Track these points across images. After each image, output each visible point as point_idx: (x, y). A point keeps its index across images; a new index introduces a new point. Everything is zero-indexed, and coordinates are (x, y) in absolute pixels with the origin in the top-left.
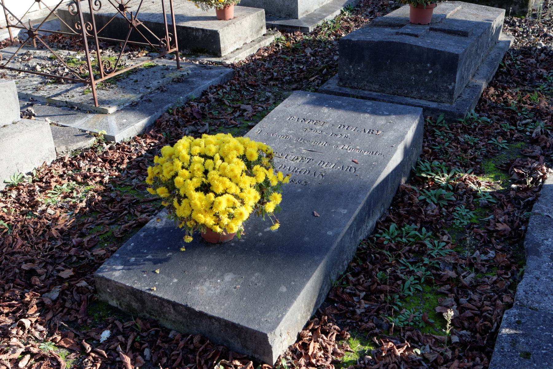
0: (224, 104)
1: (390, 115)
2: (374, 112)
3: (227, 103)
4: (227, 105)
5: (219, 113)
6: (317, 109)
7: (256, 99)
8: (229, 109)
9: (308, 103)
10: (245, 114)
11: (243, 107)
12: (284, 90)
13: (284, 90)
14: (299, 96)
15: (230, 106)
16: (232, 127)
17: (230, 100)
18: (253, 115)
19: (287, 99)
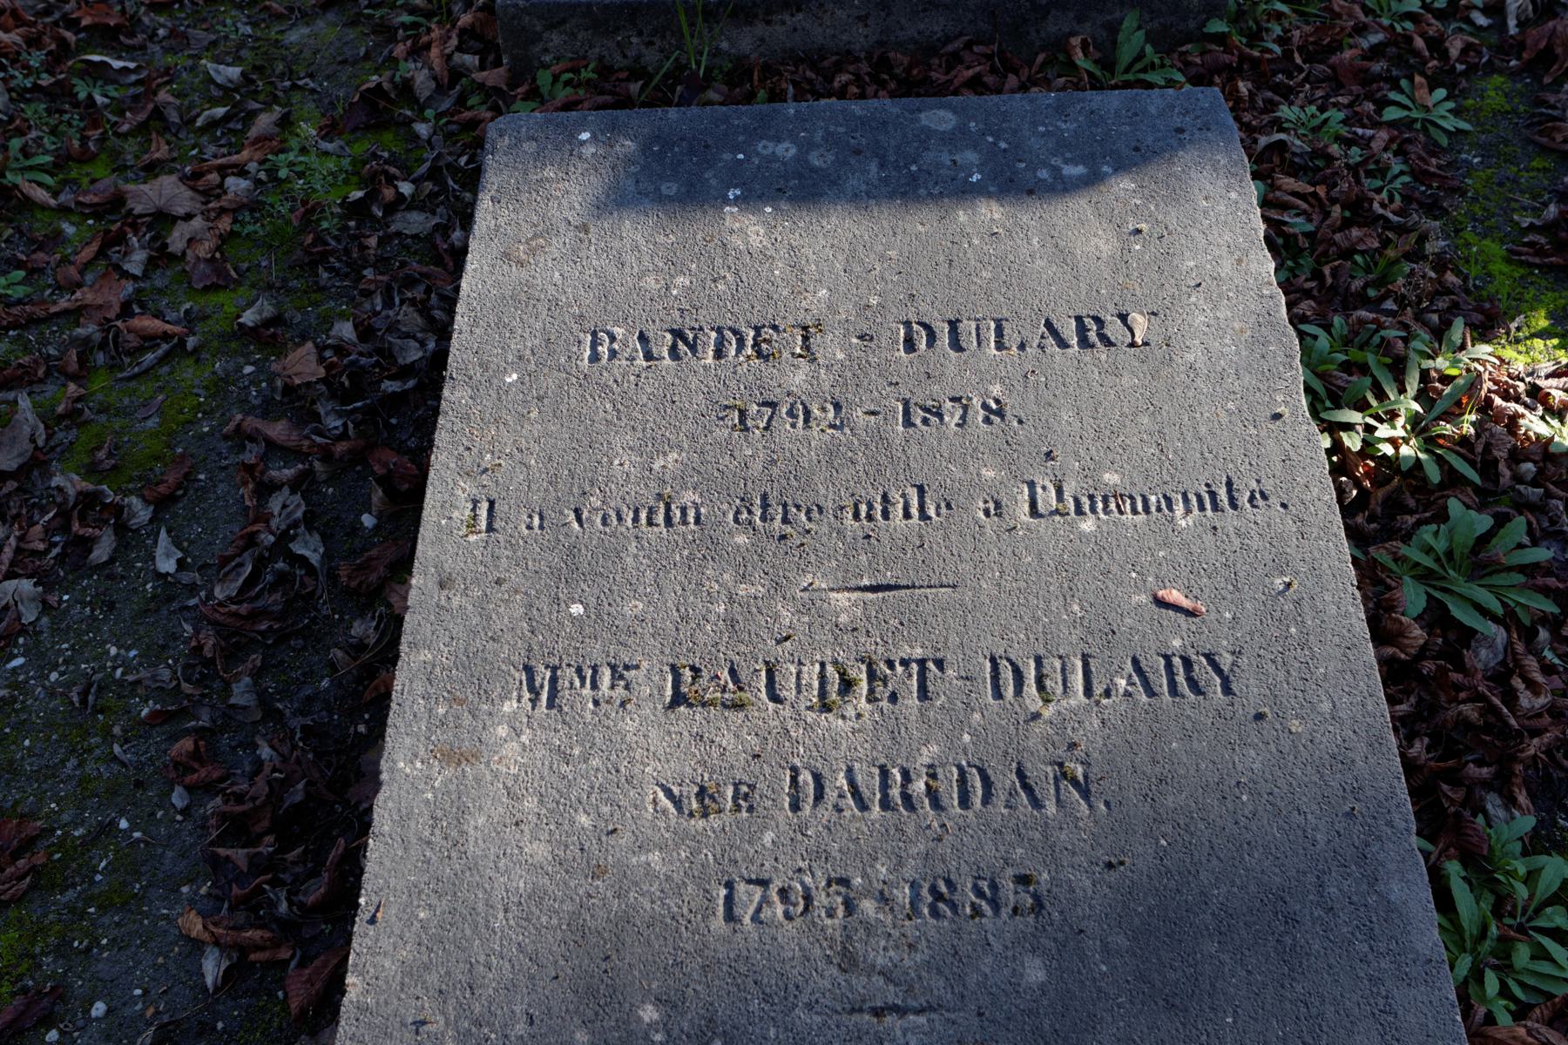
0: (28, 203)
1: (1093, 179)
2: (1013, 181)
3: (40, 195)
4: (44, 207)
5: (33, 272)
6: (698, 228)
7: (174, 117)
8: (69, 229)
9: (615, 201)
10: (176, 240)
11: (149, 194)
12: (279, 17)
13: (279, 17)
14: (540, 158)
15: (64, 210)
16: (161, 361)
17: (41, 168)
18: (226, 239)
19: (485, 205)
